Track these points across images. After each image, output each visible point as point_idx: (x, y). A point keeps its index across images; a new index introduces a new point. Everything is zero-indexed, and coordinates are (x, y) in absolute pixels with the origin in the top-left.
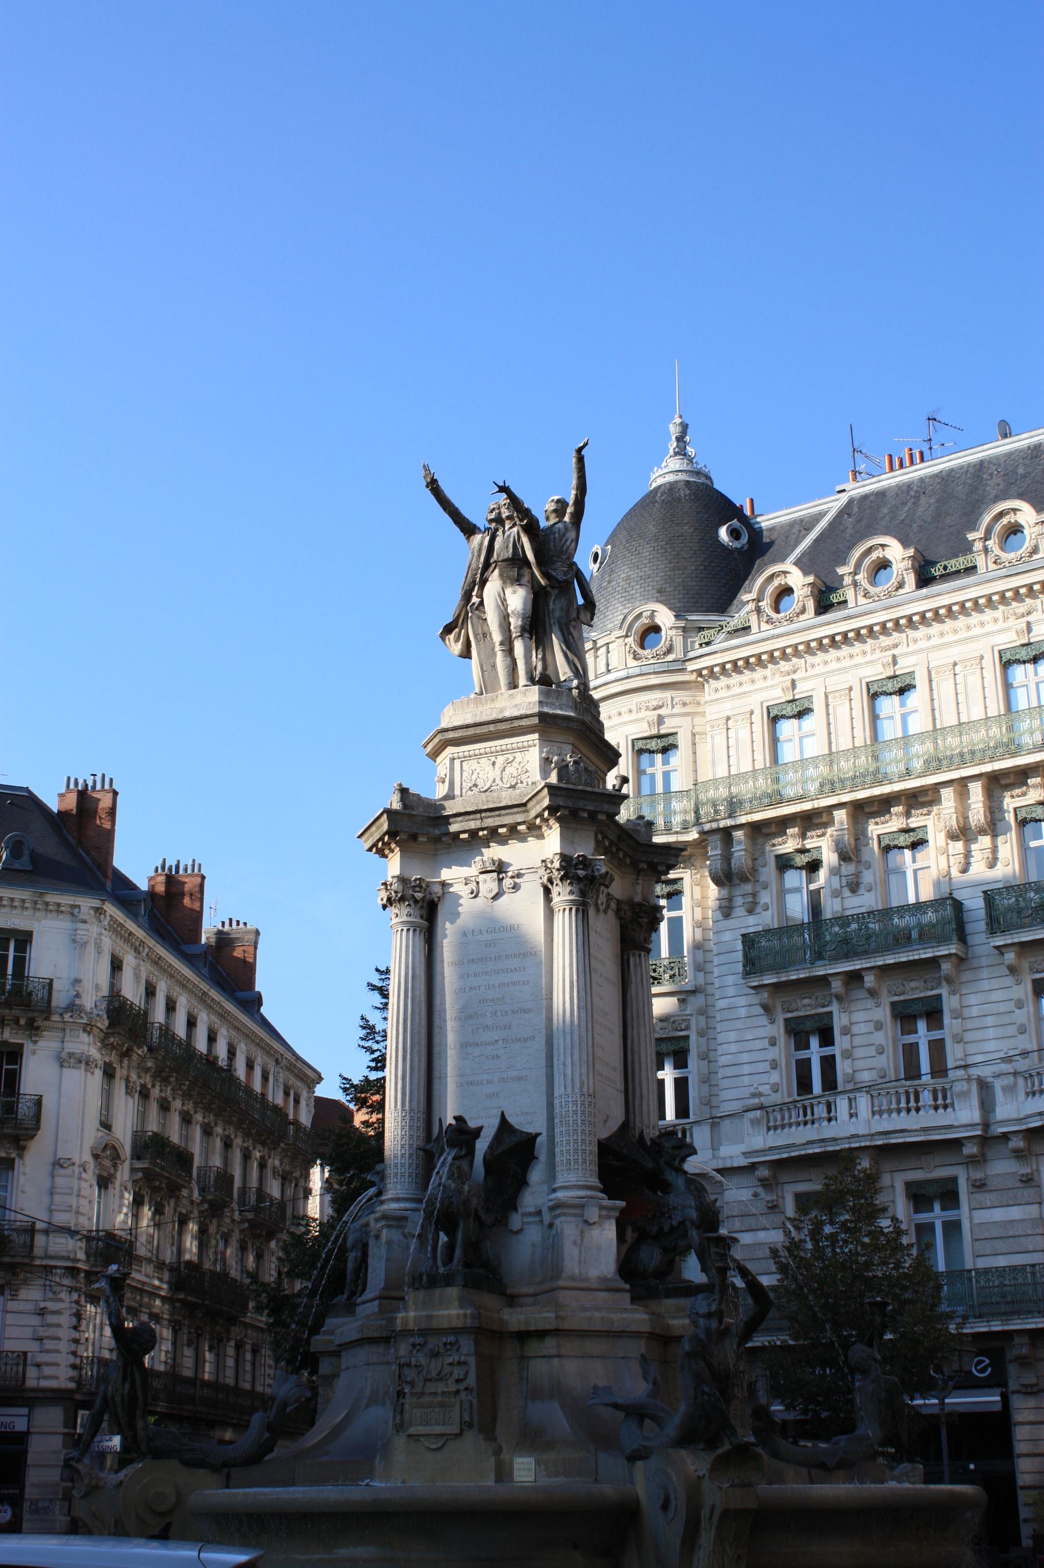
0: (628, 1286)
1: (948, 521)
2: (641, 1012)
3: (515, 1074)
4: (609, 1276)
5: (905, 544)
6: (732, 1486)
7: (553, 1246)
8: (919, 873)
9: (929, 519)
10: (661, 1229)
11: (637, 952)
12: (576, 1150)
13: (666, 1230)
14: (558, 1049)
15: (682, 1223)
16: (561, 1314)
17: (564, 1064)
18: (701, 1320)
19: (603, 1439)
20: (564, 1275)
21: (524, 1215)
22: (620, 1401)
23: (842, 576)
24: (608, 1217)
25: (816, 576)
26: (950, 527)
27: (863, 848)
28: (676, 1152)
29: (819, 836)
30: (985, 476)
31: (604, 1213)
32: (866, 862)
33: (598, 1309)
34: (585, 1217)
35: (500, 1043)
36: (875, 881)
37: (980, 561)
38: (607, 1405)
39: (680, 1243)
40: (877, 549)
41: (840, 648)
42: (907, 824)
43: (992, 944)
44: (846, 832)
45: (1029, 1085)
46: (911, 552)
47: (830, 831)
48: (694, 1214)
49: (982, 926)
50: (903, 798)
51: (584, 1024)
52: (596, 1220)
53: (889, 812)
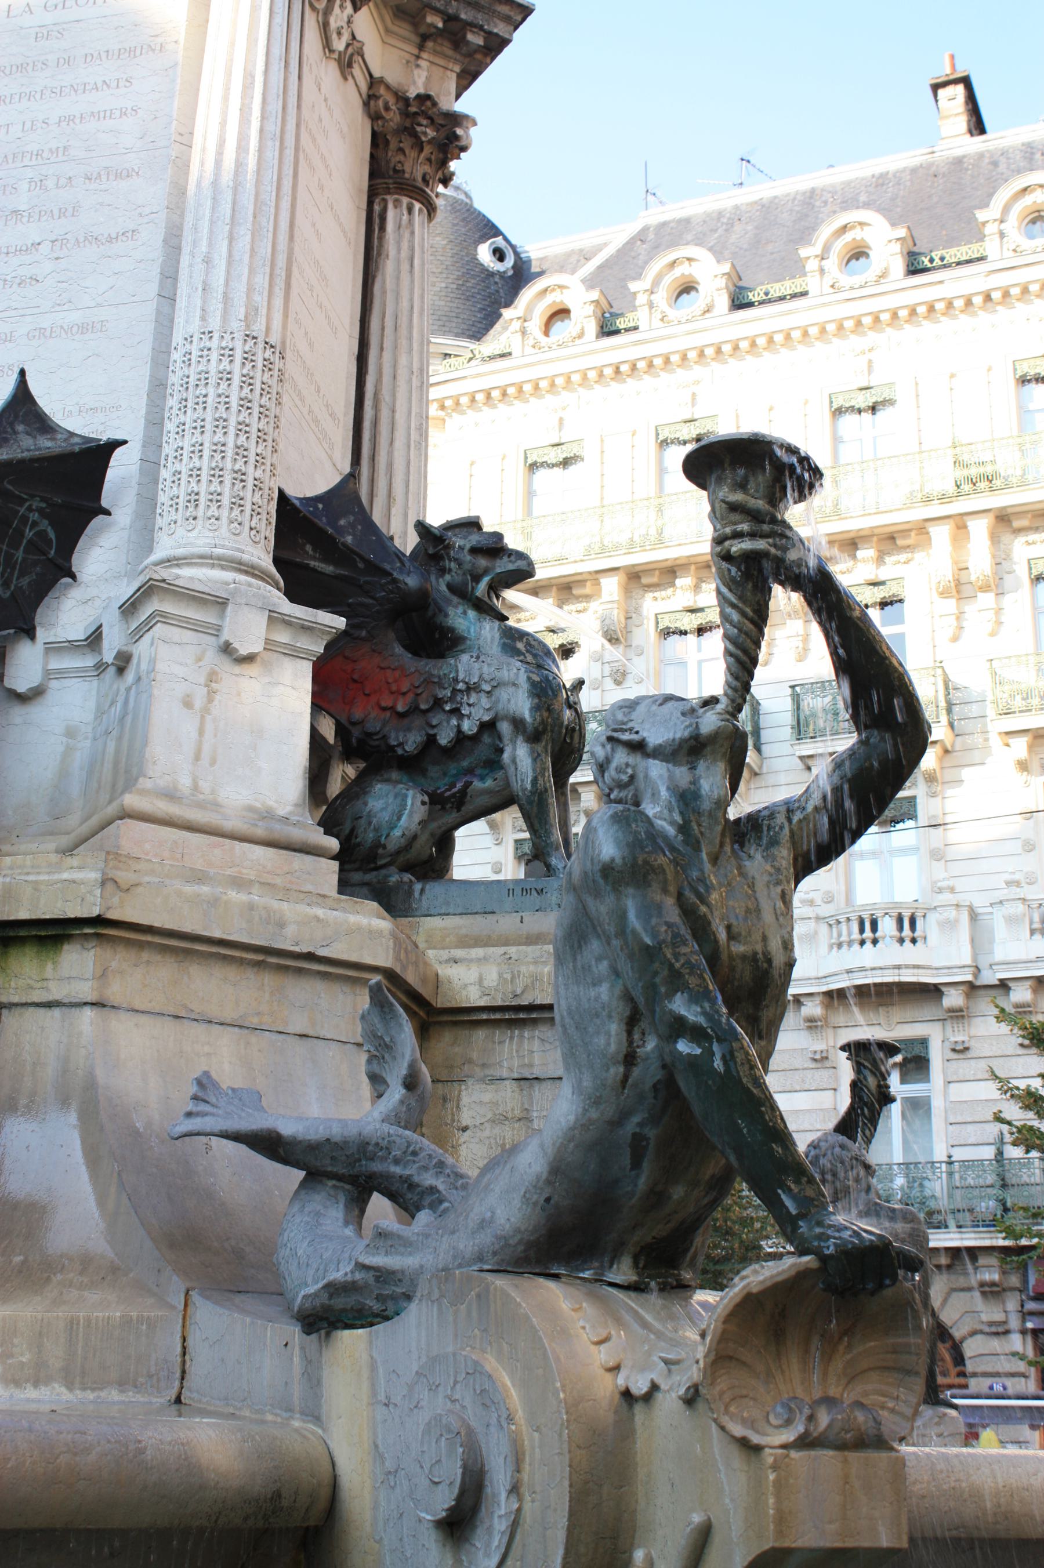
0: (333, 844)
1: (770, 248)
2: (404, 321)
3: (75, 317)
4: (282, 811)
5: (718, 254)
6: (805, 1442)
7: (122, 719)
8: (703, 664)
9: (745, 246)
10: (431, 740)
11: (405, 200)
12: (218, 472)
13: (444, 740)
14: (196, 228)
15: (489, 727)
16: (124, 876)
17: (208, 261)
18: (656, 770)
19: (217, 1260)
20: (144, 783)
21: (53, 649)
22: (287, 1129)
23: (635, 294)
24: (294, 653)
25: (602, 292)
26: (772, 253)
27: (634, 629)
28: (483, 562)
29: (579, 612)
30: (818, 204)
31: (283, 636)
32: (637, 647)
33: (239, 883)
34: (225, 636)
35: (45, 248)
36: (648, 671)
37: (812, 283)
38: (236, 1137)
39: (477, 784)
40: (682, 263)
41: (625, 382)
42: (695, 602)
43: (798, 753)
44: (615, 605)
45: (835, 934)
46: (726, 267)
47: (594, 606)
48: (520, 703)
49: (787, 732)
50: (693, 567)
51: (270, 175)
52: (257, 647)
53: (673, 585)
